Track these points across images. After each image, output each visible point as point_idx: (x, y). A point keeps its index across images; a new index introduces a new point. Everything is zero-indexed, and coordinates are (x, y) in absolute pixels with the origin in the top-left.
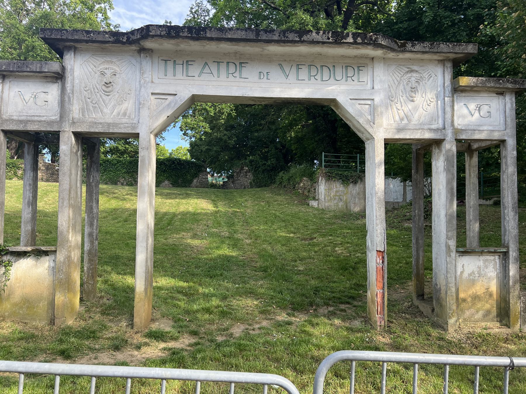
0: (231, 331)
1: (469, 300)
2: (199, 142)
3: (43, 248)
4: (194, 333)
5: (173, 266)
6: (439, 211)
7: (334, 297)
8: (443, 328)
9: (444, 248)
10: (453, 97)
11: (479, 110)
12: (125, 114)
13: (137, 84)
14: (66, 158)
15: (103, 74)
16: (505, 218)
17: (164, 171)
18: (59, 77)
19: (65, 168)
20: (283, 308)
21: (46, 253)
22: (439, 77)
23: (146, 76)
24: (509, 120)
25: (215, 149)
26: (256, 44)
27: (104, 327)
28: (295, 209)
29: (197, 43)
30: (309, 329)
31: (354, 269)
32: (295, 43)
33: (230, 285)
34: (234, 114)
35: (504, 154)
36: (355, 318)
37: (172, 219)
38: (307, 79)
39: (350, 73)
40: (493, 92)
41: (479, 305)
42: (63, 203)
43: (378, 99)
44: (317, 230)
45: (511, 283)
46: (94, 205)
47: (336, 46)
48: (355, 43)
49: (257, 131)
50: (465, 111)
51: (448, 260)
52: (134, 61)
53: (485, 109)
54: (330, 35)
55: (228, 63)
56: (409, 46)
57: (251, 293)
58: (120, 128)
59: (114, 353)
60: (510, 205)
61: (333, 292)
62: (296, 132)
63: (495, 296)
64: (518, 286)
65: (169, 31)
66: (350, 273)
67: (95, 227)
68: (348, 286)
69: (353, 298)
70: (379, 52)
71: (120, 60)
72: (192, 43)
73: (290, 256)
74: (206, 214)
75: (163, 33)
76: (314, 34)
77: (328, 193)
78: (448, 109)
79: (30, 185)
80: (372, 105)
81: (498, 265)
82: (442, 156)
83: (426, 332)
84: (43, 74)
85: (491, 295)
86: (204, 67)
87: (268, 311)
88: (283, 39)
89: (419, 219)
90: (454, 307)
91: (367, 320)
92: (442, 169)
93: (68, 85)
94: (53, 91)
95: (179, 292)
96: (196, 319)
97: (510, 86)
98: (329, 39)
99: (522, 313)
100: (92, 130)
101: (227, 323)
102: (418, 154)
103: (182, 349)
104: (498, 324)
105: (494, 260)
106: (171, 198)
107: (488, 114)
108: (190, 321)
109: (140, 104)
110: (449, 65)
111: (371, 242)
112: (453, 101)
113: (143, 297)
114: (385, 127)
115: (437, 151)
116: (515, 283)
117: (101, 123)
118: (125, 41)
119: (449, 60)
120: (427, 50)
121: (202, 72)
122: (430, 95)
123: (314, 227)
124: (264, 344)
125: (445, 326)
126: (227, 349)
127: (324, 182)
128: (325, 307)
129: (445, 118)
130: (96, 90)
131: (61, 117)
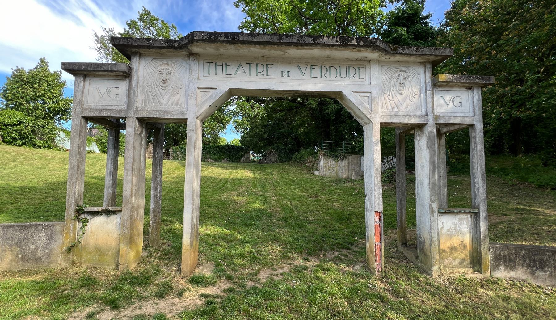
0: (260, 276)
1: (448, 250)
2: (246, 136)
3: (111, 209)
4: (229, 278)
5: (221, 217)
6: (423, 180)
7: (337, 243)
8: (427, 273)
9: (427, 208)
10: (433, 90)
11: (453, 101)
12: (177, 104)
13: (187, 80)
14: (131, 138)
15: (161, 73)
16: (475, 186)
17: (224, 153)
18: (126, 75)
19: (130, 145)
20: (300, 253)
21: (115, 213)
22: (419, 77)
23: (193, 74)
24: (477, 109)
25: (255, 140)
26: (279, 47)
27: (158, 272)
28: (305, 176)
29: (233, 47)
30: (321, 274)
31: (348, 219)
32: (310, 46)
33: (260, 233)
34: (266, 116)
35: (473, 135)
36: (355, 263)
37: (226, 182)
38: (319, 77)
39: (352, 72)
40: (463, 87)
41: (456, 255)
42: (127, 173)
43: (375, 93)
44: (320, 191)
45: (482, 238)
46: (158, 174)
47: (343, 48)
48: (358, 45)
49: (280, 129)
50: (442, 102)
51: (432, 219)
52: (185, 63)
53: (457, 101)
54: (338, 39)
55: (257, 64)
56: (400, 50)
57: (275, 240)
58: (173, 114)
59: (158, 302)
60: (480, 175)
61: (336, 239)
62: (305, 129)
63: (468, 248)
64: (487, 240)
65: (210, 36)
66: (346, 223)
67: (158, 191)
68: (346, 233)
69: (351, 244)
70: (375, 55)
71: (174, 63)
72: (229, 47)
73: (303, 209)
74: (248, 179)
75: (204, 38)
76: (325, 38)
77: (326, 167)
78: (429, 100)
79: (112, 159)
80: (370, 97)
81: (470, 223)
82: (425, 136)
83: (415, 277)
84: (114, 74)
85: (465, 247)
86: (238, 68)
87: (288, 256)
88: (301, 42)
89: (402, 185)
90: (437, 257)
91: (367, 265)
92: (425, 147)
93: (134, 82)
94: (123, 86)
95: (223, 239)
96: (233, 263)
97: (478, 81)
98: (337, 42)
99: (492, 262)
100: (151, 116)
101: (256, 267)
102: (400, 136)
103: (217, 297)
104: (471, 270)
105: (467, 218)
106: (227, 169)
107: (460, 104)
108: (227, 265)
109: (189, 96)
110: (429, 66)
111: (370, 204)
112: (433, 94)
113: (189, 249)
114: (380, 113)
115: (420, 133)
116: (485, 237)
117: (158, 111)
118: (176, 46)
119: (429, 62)
120: (414, 53)
121: (237, 71)
122: (415, 89)
123: (318, 188)
124: (285, 291)
125: (430, 272)
126: (254, 298)
127: (323, 159)
128: (331, 252)
129: (427, 107)
130: (156, 86)
131: (128, 106)
